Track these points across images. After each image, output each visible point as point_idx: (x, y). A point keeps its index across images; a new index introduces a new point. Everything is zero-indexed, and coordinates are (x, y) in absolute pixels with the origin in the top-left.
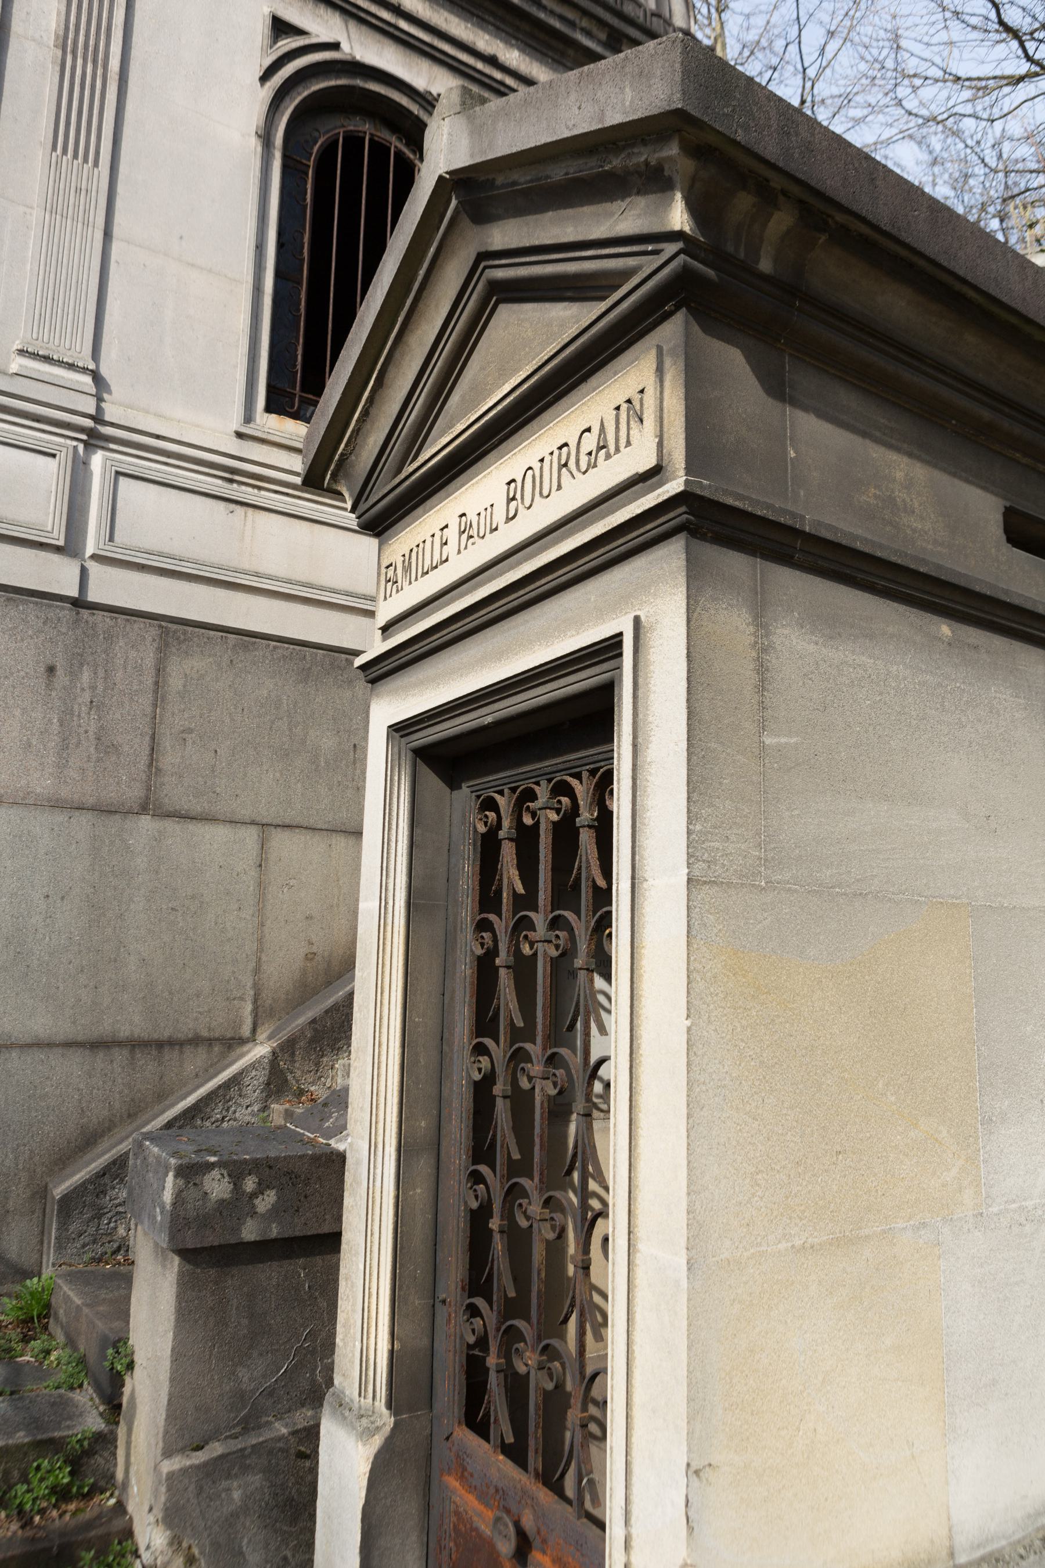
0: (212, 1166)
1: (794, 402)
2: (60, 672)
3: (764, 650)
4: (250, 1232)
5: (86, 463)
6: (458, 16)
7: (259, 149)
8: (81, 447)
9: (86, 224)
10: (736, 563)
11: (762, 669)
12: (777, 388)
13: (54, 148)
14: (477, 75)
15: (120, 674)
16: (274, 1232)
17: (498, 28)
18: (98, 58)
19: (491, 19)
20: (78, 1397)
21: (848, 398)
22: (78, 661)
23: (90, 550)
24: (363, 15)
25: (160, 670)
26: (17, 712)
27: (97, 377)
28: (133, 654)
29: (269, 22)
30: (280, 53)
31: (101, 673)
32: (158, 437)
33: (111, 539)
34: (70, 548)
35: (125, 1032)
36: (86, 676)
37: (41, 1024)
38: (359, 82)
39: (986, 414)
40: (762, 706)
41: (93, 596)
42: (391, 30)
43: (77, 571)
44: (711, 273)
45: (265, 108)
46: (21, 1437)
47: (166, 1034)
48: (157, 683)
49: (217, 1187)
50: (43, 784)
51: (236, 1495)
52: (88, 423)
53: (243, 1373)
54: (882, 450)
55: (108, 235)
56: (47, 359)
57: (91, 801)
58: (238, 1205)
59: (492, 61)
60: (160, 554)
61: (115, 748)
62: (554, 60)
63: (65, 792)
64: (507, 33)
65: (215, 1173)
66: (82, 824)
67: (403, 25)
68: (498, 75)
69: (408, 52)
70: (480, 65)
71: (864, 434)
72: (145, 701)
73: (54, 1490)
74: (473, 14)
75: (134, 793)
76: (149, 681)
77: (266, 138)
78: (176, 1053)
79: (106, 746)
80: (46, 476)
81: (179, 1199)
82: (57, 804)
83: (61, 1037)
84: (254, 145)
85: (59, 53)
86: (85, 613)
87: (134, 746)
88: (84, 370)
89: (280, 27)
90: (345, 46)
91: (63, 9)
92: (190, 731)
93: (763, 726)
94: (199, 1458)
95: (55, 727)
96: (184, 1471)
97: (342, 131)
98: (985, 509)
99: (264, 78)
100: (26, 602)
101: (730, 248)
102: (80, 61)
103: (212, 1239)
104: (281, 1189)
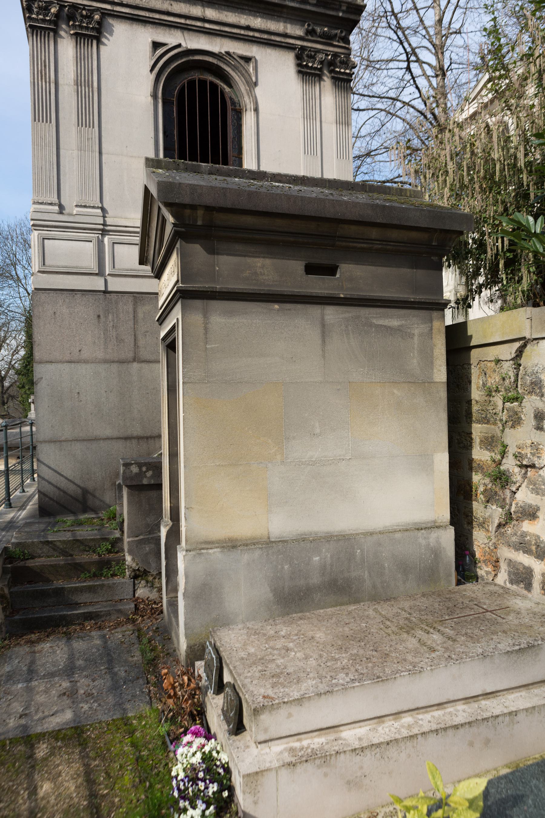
0: (133, 464)
1: (218, 254)
2: (102, 317)
3: (207, 324)
4: (145, 482)
5: (103, 241)
6: (231, 12)
7: (152, 101)
8: (100, 236)
9: (92, 151)
10: (198, 303)
11: (206, 329)
12: (212, 251)
13: (78, 125)
14: (242, 37)
15: (122, 315)
16: (152, 482)
17: (250, 11)
18: (89, 84)
19: (247, 8)
20: (116, 531)
21: (238, 247)
22: (107, 312)
23: (107, 273)
24: (189, 27)
25: (135, 312)
26: (90, 332)
27: (103, 209)
28: (125, 307)
29: (151, 45)
30: (157, 57)
31: (115, 316)
32: (126, 227)
33: (114, 267)
34: (101, 273)
35: (135, 434)
36: (110, 317)
37: (108, 432)
38: (191, 58)
39: (292, 239)
40: (206, 338)
41: (110, 289)
42: (202, 29)
43: (103, 281)
44: (183, 230)
45: (153, 83)
46: (98, 537)
47: (149, 434)
48: (134, 316)
49: (135, 469)
50: (100, 355)
51: (147, 549)
52: (101, 227)
53: (147, 519)
54: (252, 259)
55: (100, 153)
56: (85, 207)
57: (117, 359)
58: (141, 474)
59: (248, 28)
60: (131, 270)
61: (122, 341)
62: (277, 16)
63: (108, 357)
64: (255, 11)
65: (134, 466)
66: (114, 367)
67: (207, 25)
68: (251, 34)
69: (210, 36)
70: (242, 32)
71: (245, 256)
72: (131, 323)
73: (107, 549)
74: (238, 8)
75: (131, 355)
76: (131, 316)
77: (154, 96)
78: (152, 441)
79: (119, 340)
80: (90, 248)
81: (124, 472)
82: (106, 361)
83: (115, 436)
84: (150, 100)
85: (76, 87)
86: (108, 295)
87: (129, 340)
88: (98, 208)
89: (156, 45)
90: (184, 44)
91: (75, 69)
92: (147, 332)
93: (206, 343)
94: (137, 539)
95: (102, 336)
96: (132, 541)
97: (186, 81)
98: (297, 266)
99: (152, 70)
100: (87, 295)
101: (187, 222)
102: (83, 88)
103: (134, 483)
104: (153, 471)
